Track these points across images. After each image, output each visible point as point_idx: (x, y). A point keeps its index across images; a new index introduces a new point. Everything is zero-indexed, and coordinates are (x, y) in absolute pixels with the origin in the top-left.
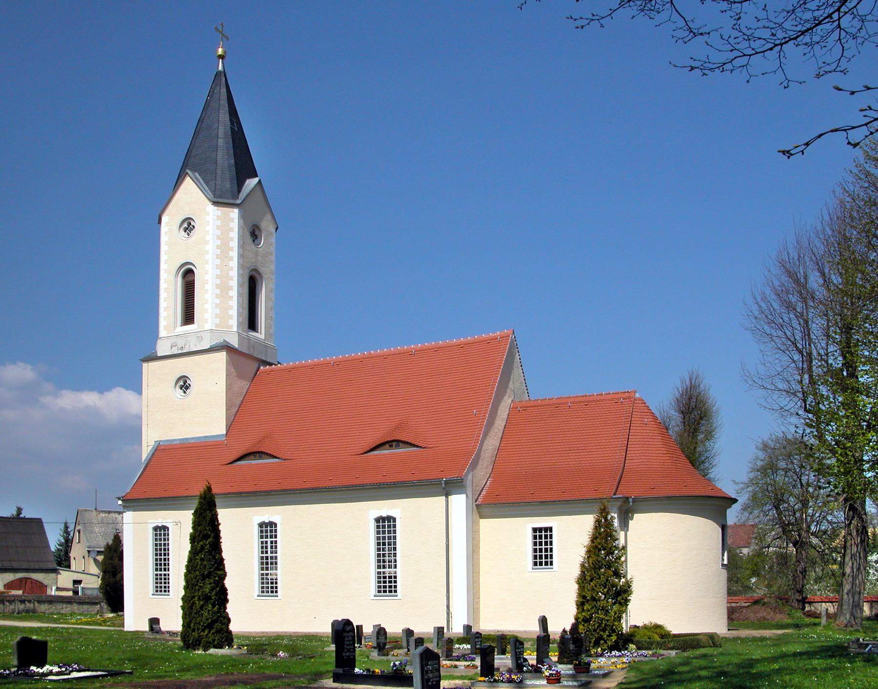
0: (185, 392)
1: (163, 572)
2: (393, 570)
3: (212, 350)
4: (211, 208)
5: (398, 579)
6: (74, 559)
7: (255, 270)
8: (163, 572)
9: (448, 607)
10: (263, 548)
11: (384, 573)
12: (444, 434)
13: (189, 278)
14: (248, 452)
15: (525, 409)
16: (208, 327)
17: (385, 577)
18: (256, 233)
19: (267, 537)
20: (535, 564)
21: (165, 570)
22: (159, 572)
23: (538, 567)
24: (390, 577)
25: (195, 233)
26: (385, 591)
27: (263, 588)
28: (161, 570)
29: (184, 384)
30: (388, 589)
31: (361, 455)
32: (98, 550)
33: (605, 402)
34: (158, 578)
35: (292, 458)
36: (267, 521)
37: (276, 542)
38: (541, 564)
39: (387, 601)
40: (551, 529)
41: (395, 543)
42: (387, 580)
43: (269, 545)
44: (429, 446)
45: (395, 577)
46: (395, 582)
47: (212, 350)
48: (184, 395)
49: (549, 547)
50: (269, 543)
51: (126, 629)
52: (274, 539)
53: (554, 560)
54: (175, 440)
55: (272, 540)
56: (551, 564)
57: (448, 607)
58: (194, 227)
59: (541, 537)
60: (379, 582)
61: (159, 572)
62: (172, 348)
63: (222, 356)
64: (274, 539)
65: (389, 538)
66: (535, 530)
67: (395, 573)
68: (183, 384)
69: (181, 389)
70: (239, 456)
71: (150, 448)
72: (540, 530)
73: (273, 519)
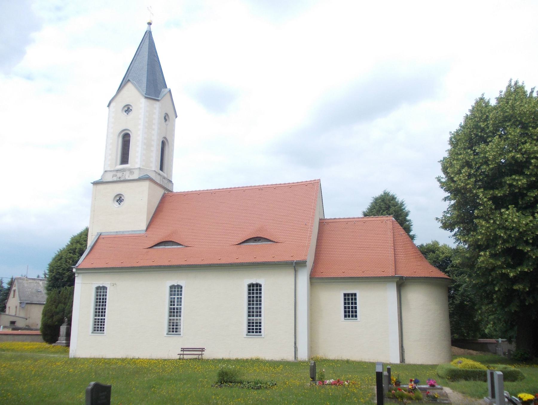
0: (119, 204)
1: (100, 318)
2: (258, 318)
3: (140, 179)
4: (143, 100)
5: (262, 324)
6: (9, 308)
7: (165, 138)
8: (100, 318)
9: (295, 343)
10: (172, 302)
11: (253, 320)
12: (205, 248)
13: (127, 139)
14: (161, 241)
15: (328, 223)
16: (137, 166)
17: (253, 323)
18: (167, 118)
19: (175, 295)
20: (345, 316)
21: (102, 316)
22: (97, 318)
23: (351, 318)
24: (257, 323)
25: (131, 114)
26: (173, 331)
27: (249, 329)
28: (99, 316)
29: (119, 199)
30: (175, 330)
31: (236, 246)
32: (26, 302)
33: (375, 222)
34: (96, 322)
35: (191, 245)
36: (176, 284)
37: (181, 298)
38: (349, 316)
39: (254, 340)
40: (355, 295)
41: (260, 301)
42: (255, 324)
43: (176, 300)
44: (279, 241)
45: (260, 323)
46: (260, 326)
47: (140, 179)
48: (119, 205)
49: (103, 314)
50: (176, 299)
51: (70, 357)
52: (179, 296)
53: (358, 314)
54: (111, 232)
55: (178, 296)
56: (356, 316)
57: (295, 343)
58: (131, 110)
59: (349, 299)
60: (170, 325)
61: (97, 318)
62: (113, 177)
63: (146, 184)
64: (179, 296)
65: (257, 297)
66: (345, 295)
67: (260, 320)
68: (118, 199)
69: (117, 202)
70: (156, 243)
71: (94, 237)
72: (348, 295)
73: (180, 283)
